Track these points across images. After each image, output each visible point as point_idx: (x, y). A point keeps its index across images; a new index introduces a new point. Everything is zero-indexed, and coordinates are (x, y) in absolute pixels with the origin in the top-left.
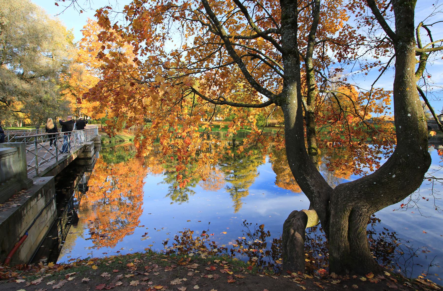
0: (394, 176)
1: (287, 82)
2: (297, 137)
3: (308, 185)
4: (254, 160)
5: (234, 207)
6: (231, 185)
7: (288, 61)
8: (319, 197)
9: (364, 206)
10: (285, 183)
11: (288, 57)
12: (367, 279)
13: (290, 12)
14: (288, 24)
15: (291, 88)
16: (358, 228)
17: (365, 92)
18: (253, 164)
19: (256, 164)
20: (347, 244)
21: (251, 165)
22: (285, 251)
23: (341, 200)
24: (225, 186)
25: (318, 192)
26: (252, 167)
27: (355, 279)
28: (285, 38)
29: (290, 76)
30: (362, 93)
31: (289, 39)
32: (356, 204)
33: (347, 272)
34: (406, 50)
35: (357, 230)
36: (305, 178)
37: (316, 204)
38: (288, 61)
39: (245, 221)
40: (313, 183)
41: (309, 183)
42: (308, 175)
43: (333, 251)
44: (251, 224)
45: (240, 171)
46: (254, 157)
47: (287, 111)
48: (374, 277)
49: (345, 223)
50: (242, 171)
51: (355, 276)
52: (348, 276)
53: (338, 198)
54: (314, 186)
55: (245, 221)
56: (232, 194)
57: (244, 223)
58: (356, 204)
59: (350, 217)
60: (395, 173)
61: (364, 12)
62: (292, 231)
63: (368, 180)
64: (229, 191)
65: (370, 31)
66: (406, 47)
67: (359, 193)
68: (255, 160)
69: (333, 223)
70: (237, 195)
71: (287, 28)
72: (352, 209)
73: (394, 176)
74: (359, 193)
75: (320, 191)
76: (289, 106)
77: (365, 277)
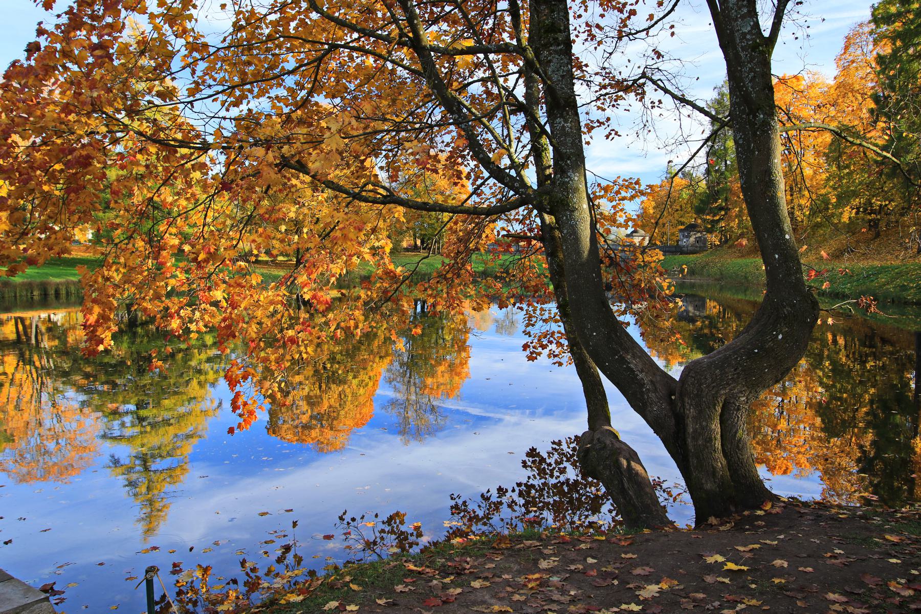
0: (780, 337)
1: (568, 165)
2: (594, 278)
3: (632, 370)
4: (206, 366)
5: (142, 523)
6: (124, 452)
7: (566, 121)
8: (655, 391)
9: (741, 392)
10: (297, 427)
11: (565, 113)
12: (765, 511)
13: (559, 19)
14: (558, 45)
15: (576, 178)
16: (736, 432)
17: (604, 184)
18: (202, 378)
19: (211, 376)
20: (724, 462)
21: (194, 382)
22: (625, 499)
23: (708, 387)
24: (106, 460)
25: (651, 381)
26: (197, 387)
27: (749, 516)
28: (553, 71)
29: (572, 153)
30: (599, 185)
31: (563, 76)
32: (731, 390)
33: (733, 509)
34: (770, 129)
35: (735, 436)
36: (624, 358)
37: (651, 404)
38: (566, 121)
39: (344, 514)
40: (640, 367)
41: (632, 366)
42: (627, 353)
43: (703, 481)
44: (363, 517)
45: (158, 404)
46: (203, 356)
47: (572, 226)
48: (772, 506)
49: (716, 426)
50: (166, 402)
51: (746, 513)
52: (736, 515)
53: (701, 384)
54: (642, 371)
55: (344, 514)
56: (131, 484)
57: (341, 518)
58: (731, 390)
59: (721, 416)
60: (781, 332)
61: (586, 10)
62: (625, 463)
63: (743, 348)
64: (119, 470)
65: (607, 55)
66: (769, 124)
67: (735, 370)
68: (207, 365)
69: (695, 431)
70: (149, 481)
71: (556, 52)
72: (725, 400)
73: (780, 337)
74: (735, 370)
75: (654, 380)
76: (576, 214)
77: (761, 509)
